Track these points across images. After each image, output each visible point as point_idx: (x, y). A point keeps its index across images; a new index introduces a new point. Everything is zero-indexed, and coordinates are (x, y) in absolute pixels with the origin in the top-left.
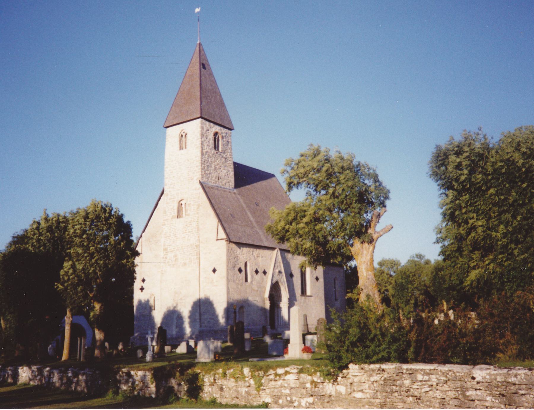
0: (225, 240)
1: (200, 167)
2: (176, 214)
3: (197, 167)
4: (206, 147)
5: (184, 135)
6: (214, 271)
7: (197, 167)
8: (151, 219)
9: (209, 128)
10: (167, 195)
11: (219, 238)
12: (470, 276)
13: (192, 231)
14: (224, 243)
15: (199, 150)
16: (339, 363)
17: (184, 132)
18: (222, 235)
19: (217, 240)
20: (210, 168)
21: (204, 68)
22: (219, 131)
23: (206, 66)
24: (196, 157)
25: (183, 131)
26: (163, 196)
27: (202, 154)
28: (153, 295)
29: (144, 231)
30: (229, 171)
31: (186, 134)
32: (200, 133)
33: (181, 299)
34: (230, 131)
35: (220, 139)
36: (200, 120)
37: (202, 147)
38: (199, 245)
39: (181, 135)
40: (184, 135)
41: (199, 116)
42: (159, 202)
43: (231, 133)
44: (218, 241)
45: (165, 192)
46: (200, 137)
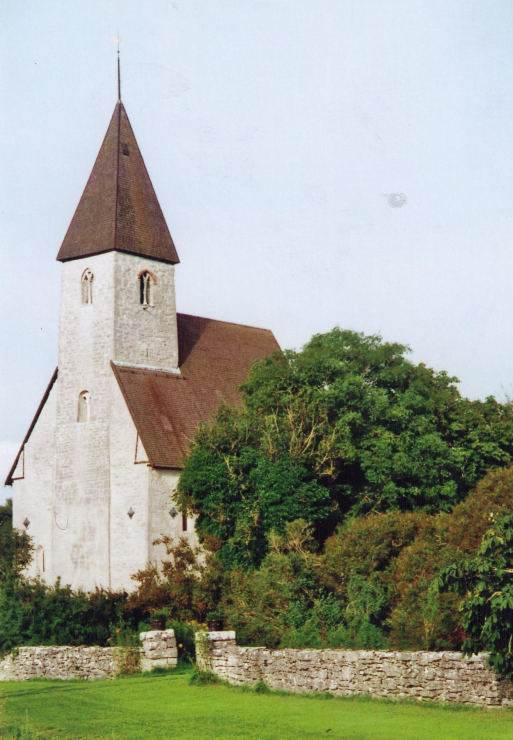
0: (147, 464)
1: (112, 337)
2: (75, 416)
3: (108, 336)
4: (123, 302)
5: (89, 277)
6: (131, 515)
7: (108, 336)
8: (39, 420)
9: (131, 266)
10: (62, 381)
11: (138, 460)
12: (329, 546)
13: (99, 446)
14: (145, 469)
15: (112, 305)
16: (13, 596)
17: (89, 273)
18: (143, 456)
19: (136, 463)
20: (130, 337)
21: (126, 153)
22: (150, 269)
23: (130, 149)
24: (107, 319)
25: (88, 271)
26: (57, 381)
27: (117, 313)
28: (42, 547)
29: (26, 440)
30: (168, 338)
31: (93, 275)
32: (113, 277)
33: (83, 557)
34: (170, 266)
35: (151, 282)
36: (113, 253)
37: (116, 302)
38: (109, 471)
39: (84, 277)
40: (89, 277)
41: (112, 246)
42: (51, 392)
43: (173, 270)
44: (137, 465)
45: (60, 376)
46: (112, 284)
